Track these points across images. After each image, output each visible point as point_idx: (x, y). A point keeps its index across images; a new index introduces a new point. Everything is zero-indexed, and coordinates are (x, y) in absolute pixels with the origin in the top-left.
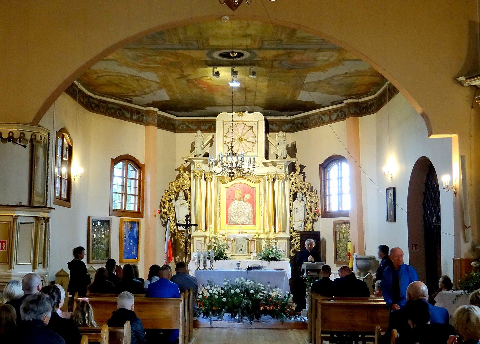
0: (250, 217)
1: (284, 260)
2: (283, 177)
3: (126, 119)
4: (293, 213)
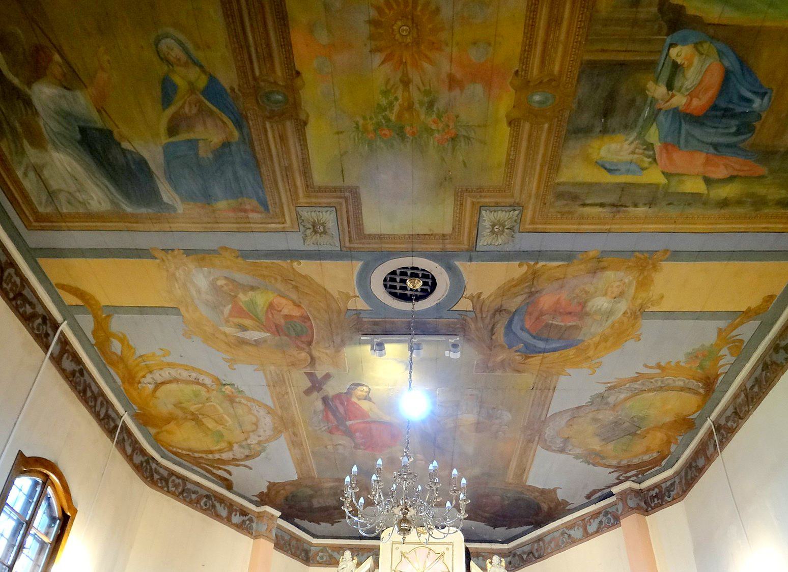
3: (218, 517)
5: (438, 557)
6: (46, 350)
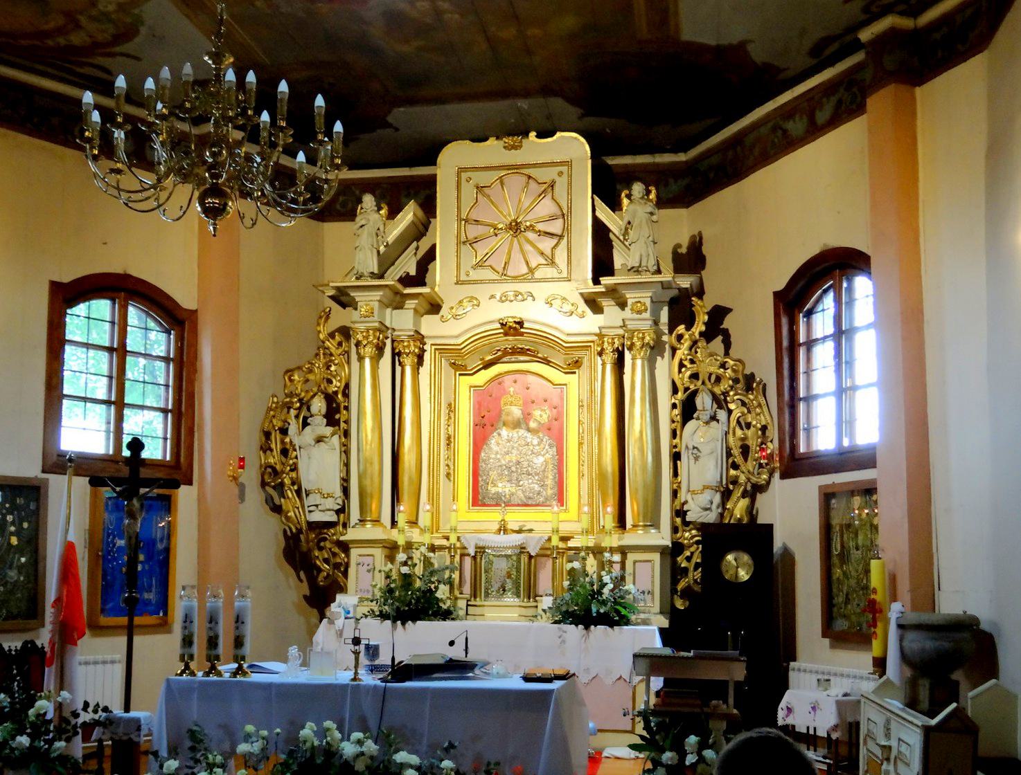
0: (550, 482)
1: (645, 622)
2: (647, 339)
4: (683, 465)
5: (543, 189)
6: (585, 296)
